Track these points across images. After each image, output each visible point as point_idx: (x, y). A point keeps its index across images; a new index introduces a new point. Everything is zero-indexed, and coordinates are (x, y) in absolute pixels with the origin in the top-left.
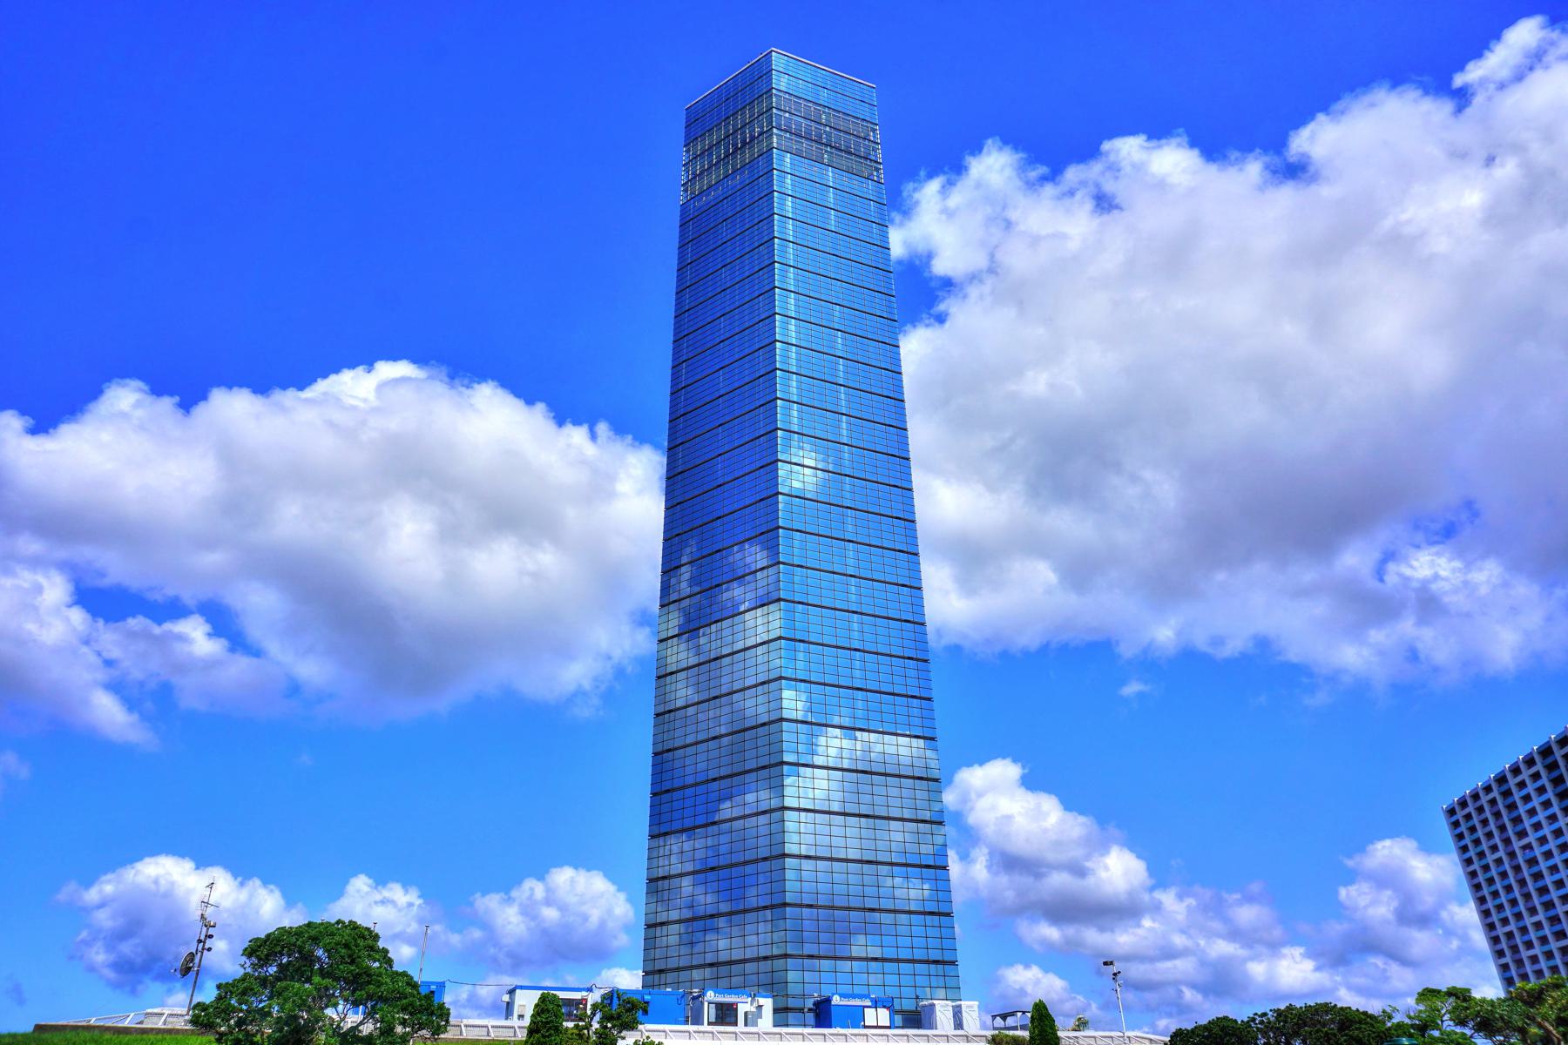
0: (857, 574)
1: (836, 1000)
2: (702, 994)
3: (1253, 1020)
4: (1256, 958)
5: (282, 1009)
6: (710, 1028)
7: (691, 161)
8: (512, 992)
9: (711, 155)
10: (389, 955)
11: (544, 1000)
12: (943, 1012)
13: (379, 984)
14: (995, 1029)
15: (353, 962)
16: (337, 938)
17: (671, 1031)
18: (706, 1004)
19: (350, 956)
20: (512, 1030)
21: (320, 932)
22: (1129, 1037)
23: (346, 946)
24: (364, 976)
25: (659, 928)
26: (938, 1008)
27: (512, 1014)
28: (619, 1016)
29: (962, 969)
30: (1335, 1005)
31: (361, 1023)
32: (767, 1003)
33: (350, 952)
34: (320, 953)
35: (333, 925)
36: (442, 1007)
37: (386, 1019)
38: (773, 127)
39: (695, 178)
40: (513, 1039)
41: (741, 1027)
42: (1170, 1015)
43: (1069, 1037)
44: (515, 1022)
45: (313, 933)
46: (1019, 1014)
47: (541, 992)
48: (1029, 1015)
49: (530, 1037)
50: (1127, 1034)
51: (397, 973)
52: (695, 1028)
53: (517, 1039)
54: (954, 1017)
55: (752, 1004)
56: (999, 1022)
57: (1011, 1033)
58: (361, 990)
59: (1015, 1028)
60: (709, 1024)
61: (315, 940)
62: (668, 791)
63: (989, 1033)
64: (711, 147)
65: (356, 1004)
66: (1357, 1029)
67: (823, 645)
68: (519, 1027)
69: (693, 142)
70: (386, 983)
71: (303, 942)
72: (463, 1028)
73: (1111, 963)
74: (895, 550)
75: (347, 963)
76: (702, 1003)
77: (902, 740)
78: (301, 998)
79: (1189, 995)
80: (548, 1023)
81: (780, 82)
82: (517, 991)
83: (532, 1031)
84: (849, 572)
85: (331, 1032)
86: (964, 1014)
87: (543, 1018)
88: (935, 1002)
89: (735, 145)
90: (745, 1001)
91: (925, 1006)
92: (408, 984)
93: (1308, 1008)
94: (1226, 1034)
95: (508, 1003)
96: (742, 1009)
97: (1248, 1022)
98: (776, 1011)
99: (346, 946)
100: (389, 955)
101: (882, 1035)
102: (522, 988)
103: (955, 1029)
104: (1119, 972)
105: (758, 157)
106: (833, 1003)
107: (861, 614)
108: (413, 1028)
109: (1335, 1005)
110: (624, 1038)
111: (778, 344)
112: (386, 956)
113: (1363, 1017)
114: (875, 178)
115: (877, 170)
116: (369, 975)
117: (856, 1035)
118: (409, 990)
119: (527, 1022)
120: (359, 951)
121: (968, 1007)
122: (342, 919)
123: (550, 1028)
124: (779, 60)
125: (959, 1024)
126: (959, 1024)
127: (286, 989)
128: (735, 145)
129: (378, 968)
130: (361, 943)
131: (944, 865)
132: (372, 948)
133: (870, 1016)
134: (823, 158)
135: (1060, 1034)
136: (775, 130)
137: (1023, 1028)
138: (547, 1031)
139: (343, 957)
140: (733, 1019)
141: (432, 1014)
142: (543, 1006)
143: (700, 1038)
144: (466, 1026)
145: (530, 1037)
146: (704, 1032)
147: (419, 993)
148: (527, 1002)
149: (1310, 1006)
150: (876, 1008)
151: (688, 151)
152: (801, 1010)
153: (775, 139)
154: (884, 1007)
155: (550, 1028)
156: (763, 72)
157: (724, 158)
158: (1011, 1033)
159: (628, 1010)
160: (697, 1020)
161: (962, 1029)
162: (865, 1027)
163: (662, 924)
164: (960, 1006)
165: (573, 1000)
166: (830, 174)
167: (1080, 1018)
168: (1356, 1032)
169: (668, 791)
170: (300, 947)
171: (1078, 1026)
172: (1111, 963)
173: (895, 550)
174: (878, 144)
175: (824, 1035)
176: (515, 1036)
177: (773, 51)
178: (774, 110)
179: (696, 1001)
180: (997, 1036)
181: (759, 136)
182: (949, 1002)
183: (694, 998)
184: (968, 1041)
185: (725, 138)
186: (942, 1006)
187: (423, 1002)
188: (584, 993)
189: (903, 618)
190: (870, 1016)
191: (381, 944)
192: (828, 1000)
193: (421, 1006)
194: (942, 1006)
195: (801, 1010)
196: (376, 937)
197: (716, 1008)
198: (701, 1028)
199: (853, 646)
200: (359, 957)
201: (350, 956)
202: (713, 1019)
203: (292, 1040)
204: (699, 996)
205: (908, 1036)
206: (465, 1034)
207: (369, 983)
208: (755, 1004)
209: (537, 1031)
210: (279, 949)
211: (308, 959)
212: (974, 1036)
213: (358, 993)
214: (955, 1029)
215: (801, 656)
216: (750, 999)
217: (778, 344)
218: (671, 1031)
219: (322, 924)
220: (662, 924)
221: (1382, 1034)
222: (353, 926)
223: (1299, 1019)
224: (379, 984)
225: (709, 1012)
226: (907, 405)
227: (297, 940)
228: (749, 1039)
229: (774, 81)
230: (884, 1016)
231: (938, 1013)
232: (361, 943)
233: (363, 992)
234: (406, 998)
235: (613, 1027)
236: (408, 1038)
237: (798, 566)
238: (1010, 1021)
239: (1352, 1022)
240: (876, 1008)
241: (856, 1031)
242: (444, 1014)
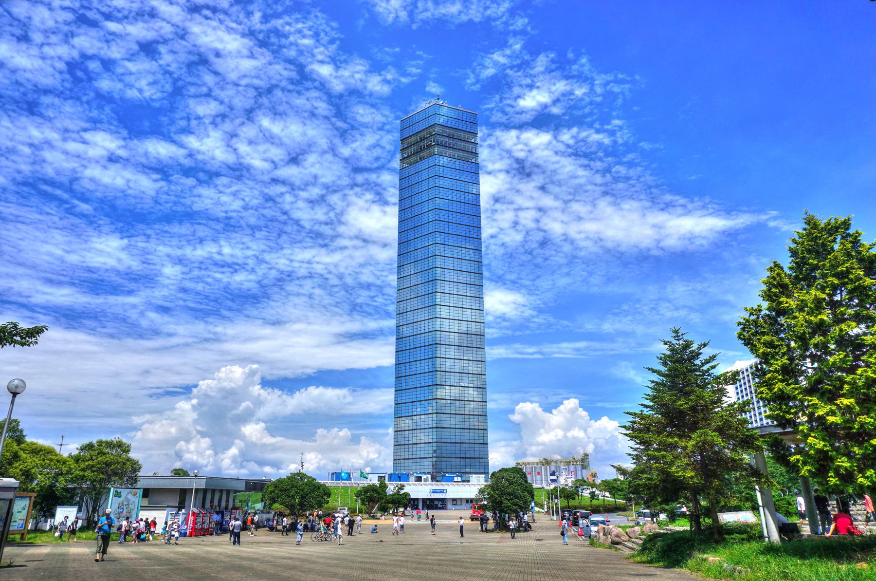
96: (423, 478)
133: (456, 479)
190: (456, 479)
230: (459, 479)
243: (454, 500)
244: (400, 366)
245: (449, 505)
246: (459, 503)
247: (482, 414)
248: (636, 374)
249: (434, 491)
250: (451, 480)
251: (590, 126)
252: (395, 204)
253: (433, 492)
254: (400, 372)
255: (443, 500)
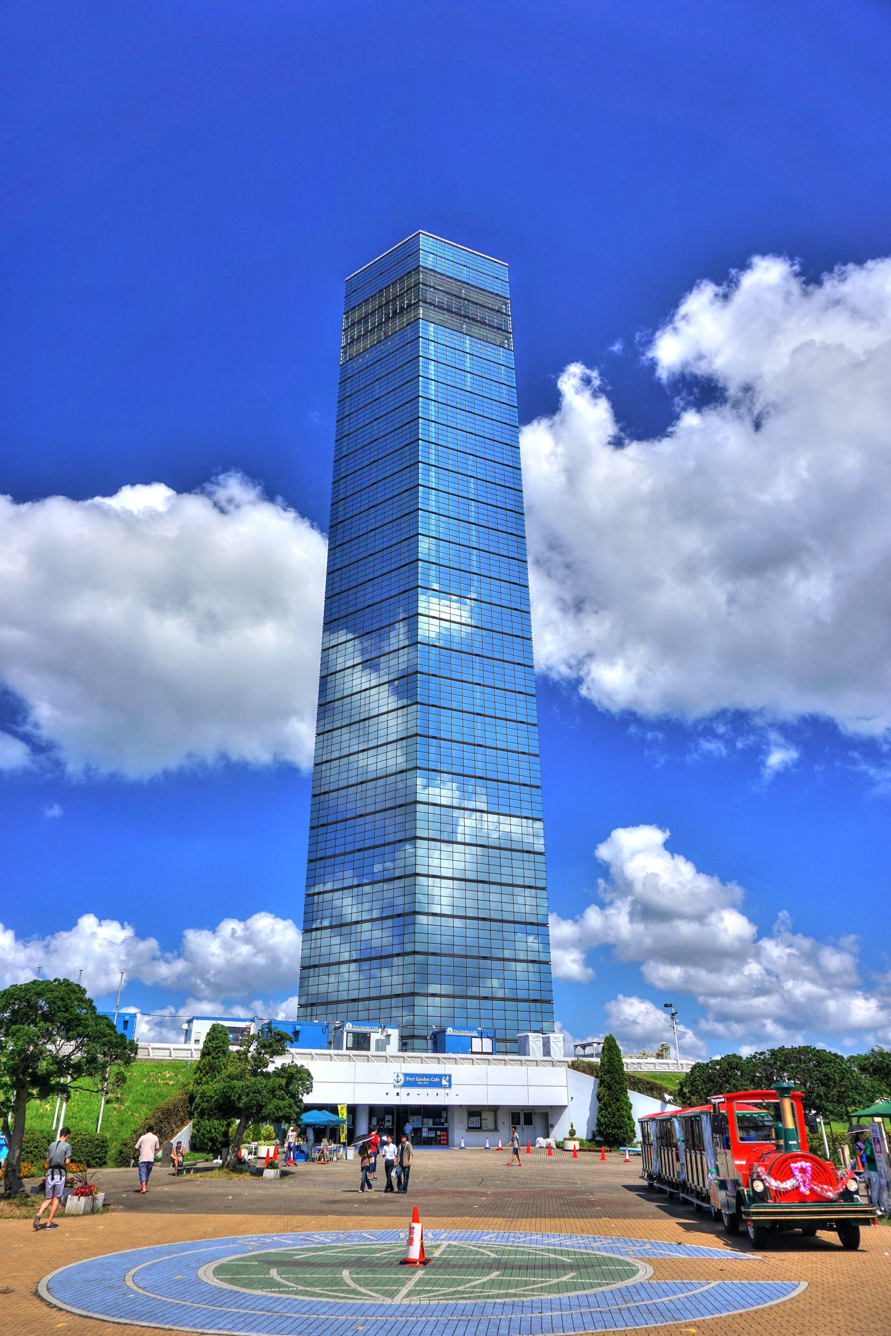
0: (482, 683)
1: (450, 1031)
2: (342, 1026)
3: (755, 1057)
4: (834, 996)
5: (16, 1045)
6: (348, 1052)
7: (350, 327)
8: (190, 1022)
9: (366, 322)
10: (93, 1004)
11: (214, 1030)
12: (535, 1042)
13: (86, 1027)
14: (576, 1056)
15: (67, 1010)
16: (56, 994)
17: (316, 1054)
18: (345, 1033)
19: (64, 1006)
20: (190, 1052)
21: (43, 989)
22: (682, 1065)
23: (62, 999)
24: (75, 1021)
25: (312, 970)
26: (531, 1039)
27: (190, 1040)
28: (270, 1046)
29: (556, 1007)
30: (815, 1048)
31: (72, 1053)
32: (394, 1033)
33: (65, 1004)
34: (42, 1003)
35: (52, 983)
36: (132, 1043)
37: (91, 1052)
38: (419, 300)
39: (352, 342)
40: (190, 1059)
41: (373, 1051)
42: (752, 1043)
43: (633, 1063)
44: (192, 1045)
45: (38, 989)
46: (595, 1045)
47: (214, 1022)
48: (602, 1045)
49: (203, 1059)
50: (680, 1062)
51: (99, 1017)
52: (336, 1052)
53: (193, 1059)
54: (544, 1045)
55: (382, 1034)
56: (580, 1051)
57: (586, 1059)
58: (72, 1031)
59: (591, 1056)
60: (347, 1049)
61: (39, 995)
62: (321, 859)
63: (570, 1059)
64: (366, 316)
65: (69, 1039)
66: (826, 1066)
67: (452, 741)
68: (196, 1050)
69: (351, 310)
70: (91, 1024)
71: (31, 996)
72: (151, 1050)
73: (671, 1006)
74: (514, 663)
75: (63, 1011)
76: (342, 1032)
77: (514, 821)
78: (29, 1038)
79: (770, 1027)
80: (217, 1048)
81: (427, 260)
82: (195, 1021)
83: (204, 1054)
84: (475, 681)
85: (51, 1061)
86: (552, 1044)
87: (214, 1043)
88: (529, 1034)
89: (387, 314)
90: (377, 1031)
91: (522, 1037)
92: (108, 1025)
93: (793, 1049)
94: (731, 1068)
95: (187, 1030)
96: (375, 1037)
97: (751, 1058)
98: (402, 1038)
99: (62, 999)
100: (93, 1004)
101: (484, 1060)
102: (198, 1018)
103: (544, 1056)
104: (676, 1013)
105: (407, 325)
106: (447, 1034)
107: (484, 715)
108: (111, 1058)
109: (815, 1048)
110: (273, 1062)
111: (421, 488)
112: (91, 1005)
113: (833, 1057)
114: (506, 346)
115: (508, 339)
116: (79, 1020)
117: (464, 1059)
118: (108, 1031)
119: (201, 1046)
120: (72, 1002)
121: (555, 1038)
122: (58, 977)
123: (219, 1052)
124: (427, 241)
125: (547, 1053)
126: (547, 1053)
127: (18, 1031)
128: (387, 314)
129: (85, 1014)
130: (73, 997)
131: (545, 922)
132: (80, 1000)
133: (476, 1044)
134: (462, 328)
135: (624, 1060)
136: (421, 303)
137: (597, 1055)
138: (217, 1054)
139: (59, 1007)
140: (366, 1045)
141: (125, 1048)
142: (213, 1034)
143: (339, 1060)
144: (153, 1049)
145: (203, 1059)
146: (342, 1055)
147: (115, 1032)
148: (201, 1029)
149: (795, 1048)
150: (481, 1038)
151: (347, 318)
152: (425, 1038)
153: (421, 311)
154: (488, 1037)
155: (219, 1052)
156: (413, 250)
157: (378, 325)
158: (586, 1059)
159: (278, 1041)
160: (339, 1047)
161: (550, 1056)
162: (472, 1053)
163: (315, 966)
164: (549, 1038)
165: (239, 1028)
166: (468, 342)
167: (663, 1045)
168: (825, 1069)
169: (321, 859)
170: (28, 999)
171: (662, 1051)
172: (671, 1006)
173: (514, 663)
174: (509, 316)
175: (438, 1058)
176: (192, 1057)
177: (420, 233)
178: (421, 286)
179: (338, 1031)
180: (576, 1062)
181: (407, 307)
182: (540, 1035)
183: (336, 1029)
184: (553, 1066)
185: (379, 308)
186: (534, 1037)
187: (119, 1040)
188: (248, 1023)
189: (519, 719)
190: (476, 1044)
191: (87, 996)
192: (444, 1031)
193: (116, 1042)
194: (534, 1037)
195: (425, 1038)
196: (84, 991)
197: (354, 1037)
198: (340, 1052)
199: (476, 743)
200: (72, 1007)
201: (64, 1006)
202: (350, 1045)
203: (22, 1067)
204: (340, 1027)
205: (505, 1060)
206: (151, 1055)
207: (79, 1025)
208: (385, 1034)
209: (209, 1054)
210: (12, 1001)
211: (34, 1007)
212: (558, 1062)
213: (71, 1033)
214: (544, 1056)
215: (433, 750)
216: (380, 1030)
217: (421, 488)
218: (316, 1054)
219: (44, 982)
220: (315, 966)
221: (844, 1071)
222: (66, 983)
223: (786, 1058)
224: (86, 1027)
225: (347, 1040)
226: (528, 541)
227: (26, 995)
228: (378, 1061)
229: (421, 259)
230: (487, 1045)
231: (531, 1043)
232: (73, 997)
233: (74, 1032)
234: (105, 1037)
235: (266, 1053)
236: (107, 1065)
237: (433, 675)
238: (588, 1050)
239: (825, 1061)
240: (481, 1038)
241: (464, 1056)
242: (134, 1048)
243: (474, 1112)
244: (321, 830)
245: (459, 1133)
246: (488, 1122)
247: (534, 995)
248: (880, 1161)
249: (411, 1081)
250: (465, 1047)
251: (502, 1193)
252: (410, 1216)
253: (407, 1084)
254: (320, 846)
255: (437, 1113)
